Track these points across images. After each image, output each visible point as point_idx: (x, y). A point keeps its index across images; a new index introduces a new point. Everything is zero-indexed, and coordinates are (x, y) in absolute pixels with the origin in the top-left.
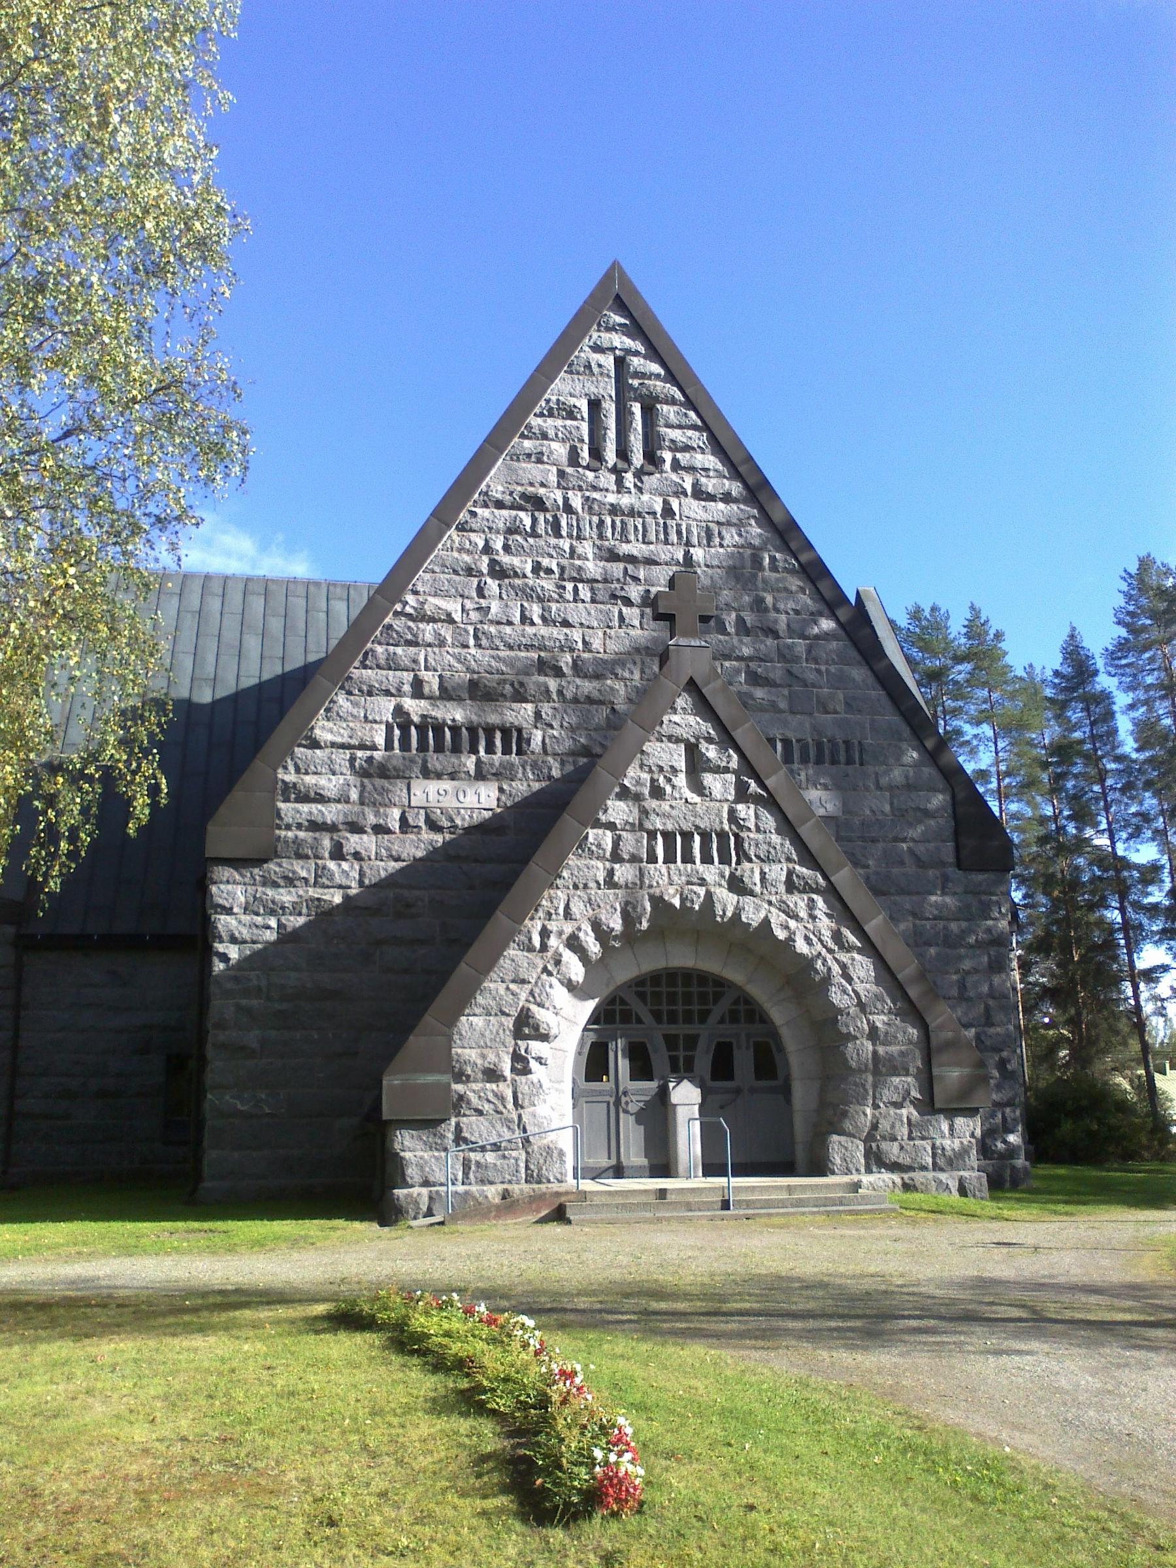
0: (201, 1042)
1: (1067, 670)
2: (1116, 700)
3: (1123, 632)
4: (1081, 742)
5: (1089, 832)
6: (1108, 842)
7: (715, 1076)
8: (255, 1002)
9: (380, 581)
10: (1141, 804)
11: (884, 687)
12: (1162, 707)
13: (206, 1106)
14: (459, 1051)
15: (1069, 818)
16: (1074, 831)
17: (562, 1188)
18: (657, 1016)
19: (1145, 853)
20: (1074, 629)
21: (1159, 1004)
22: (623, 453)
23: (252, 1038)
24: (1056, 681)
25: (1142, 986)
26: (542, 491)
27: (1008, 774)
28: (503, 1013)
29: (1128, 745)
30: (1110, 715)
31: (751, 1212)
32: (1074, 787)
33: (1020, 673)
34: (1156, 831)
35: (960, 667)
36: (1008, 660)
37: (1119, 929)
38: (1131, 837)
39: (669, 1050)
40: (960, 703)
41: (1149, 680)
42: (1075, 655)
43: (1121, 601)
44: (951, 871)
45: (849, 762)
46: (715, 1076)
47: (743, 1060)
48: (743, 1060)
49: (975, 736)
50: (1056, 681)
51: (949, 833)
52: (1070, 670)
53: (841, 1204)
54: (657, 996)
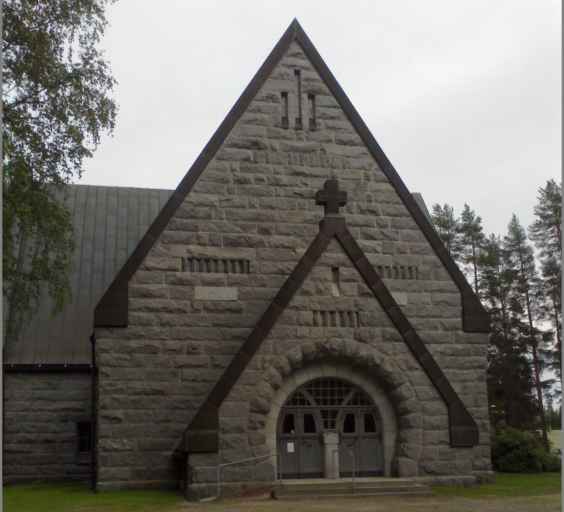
0: (94, 415)
2: (535, 252)
3: (538, 218)
5: (519, 316)
6: (528, 321)
8: (121, 396)
9: (175, 188)
12: (556, 255)
13: (98, 446)
15: (510, 309)
16: (512, 316)
17: (273, 483)
19: (546, 326)
20: (514, 216)
21: (549, 398)
22: (299, 120)
23: (119, 413)
24: (505, 242)
25: (542, 390)
26: (259, 139)
27: (481, 287)
29: (540, 275)
30: (531, 258)
31: (365, 494)
32: (513, 294)
34: (551, 315)
35: (458, 235)
37: (532, 363)
38: (539, 318)
40: (458, 253)
41: (550, 242)
42: (515, 228)
44: (461, 333)
45: (411, 278)
47: (359, 423)
48: (359, 423)
49: (466, 269)
50: (505, 242)
51: (459, 313)
52: (512, 236)
54: (317, 393)
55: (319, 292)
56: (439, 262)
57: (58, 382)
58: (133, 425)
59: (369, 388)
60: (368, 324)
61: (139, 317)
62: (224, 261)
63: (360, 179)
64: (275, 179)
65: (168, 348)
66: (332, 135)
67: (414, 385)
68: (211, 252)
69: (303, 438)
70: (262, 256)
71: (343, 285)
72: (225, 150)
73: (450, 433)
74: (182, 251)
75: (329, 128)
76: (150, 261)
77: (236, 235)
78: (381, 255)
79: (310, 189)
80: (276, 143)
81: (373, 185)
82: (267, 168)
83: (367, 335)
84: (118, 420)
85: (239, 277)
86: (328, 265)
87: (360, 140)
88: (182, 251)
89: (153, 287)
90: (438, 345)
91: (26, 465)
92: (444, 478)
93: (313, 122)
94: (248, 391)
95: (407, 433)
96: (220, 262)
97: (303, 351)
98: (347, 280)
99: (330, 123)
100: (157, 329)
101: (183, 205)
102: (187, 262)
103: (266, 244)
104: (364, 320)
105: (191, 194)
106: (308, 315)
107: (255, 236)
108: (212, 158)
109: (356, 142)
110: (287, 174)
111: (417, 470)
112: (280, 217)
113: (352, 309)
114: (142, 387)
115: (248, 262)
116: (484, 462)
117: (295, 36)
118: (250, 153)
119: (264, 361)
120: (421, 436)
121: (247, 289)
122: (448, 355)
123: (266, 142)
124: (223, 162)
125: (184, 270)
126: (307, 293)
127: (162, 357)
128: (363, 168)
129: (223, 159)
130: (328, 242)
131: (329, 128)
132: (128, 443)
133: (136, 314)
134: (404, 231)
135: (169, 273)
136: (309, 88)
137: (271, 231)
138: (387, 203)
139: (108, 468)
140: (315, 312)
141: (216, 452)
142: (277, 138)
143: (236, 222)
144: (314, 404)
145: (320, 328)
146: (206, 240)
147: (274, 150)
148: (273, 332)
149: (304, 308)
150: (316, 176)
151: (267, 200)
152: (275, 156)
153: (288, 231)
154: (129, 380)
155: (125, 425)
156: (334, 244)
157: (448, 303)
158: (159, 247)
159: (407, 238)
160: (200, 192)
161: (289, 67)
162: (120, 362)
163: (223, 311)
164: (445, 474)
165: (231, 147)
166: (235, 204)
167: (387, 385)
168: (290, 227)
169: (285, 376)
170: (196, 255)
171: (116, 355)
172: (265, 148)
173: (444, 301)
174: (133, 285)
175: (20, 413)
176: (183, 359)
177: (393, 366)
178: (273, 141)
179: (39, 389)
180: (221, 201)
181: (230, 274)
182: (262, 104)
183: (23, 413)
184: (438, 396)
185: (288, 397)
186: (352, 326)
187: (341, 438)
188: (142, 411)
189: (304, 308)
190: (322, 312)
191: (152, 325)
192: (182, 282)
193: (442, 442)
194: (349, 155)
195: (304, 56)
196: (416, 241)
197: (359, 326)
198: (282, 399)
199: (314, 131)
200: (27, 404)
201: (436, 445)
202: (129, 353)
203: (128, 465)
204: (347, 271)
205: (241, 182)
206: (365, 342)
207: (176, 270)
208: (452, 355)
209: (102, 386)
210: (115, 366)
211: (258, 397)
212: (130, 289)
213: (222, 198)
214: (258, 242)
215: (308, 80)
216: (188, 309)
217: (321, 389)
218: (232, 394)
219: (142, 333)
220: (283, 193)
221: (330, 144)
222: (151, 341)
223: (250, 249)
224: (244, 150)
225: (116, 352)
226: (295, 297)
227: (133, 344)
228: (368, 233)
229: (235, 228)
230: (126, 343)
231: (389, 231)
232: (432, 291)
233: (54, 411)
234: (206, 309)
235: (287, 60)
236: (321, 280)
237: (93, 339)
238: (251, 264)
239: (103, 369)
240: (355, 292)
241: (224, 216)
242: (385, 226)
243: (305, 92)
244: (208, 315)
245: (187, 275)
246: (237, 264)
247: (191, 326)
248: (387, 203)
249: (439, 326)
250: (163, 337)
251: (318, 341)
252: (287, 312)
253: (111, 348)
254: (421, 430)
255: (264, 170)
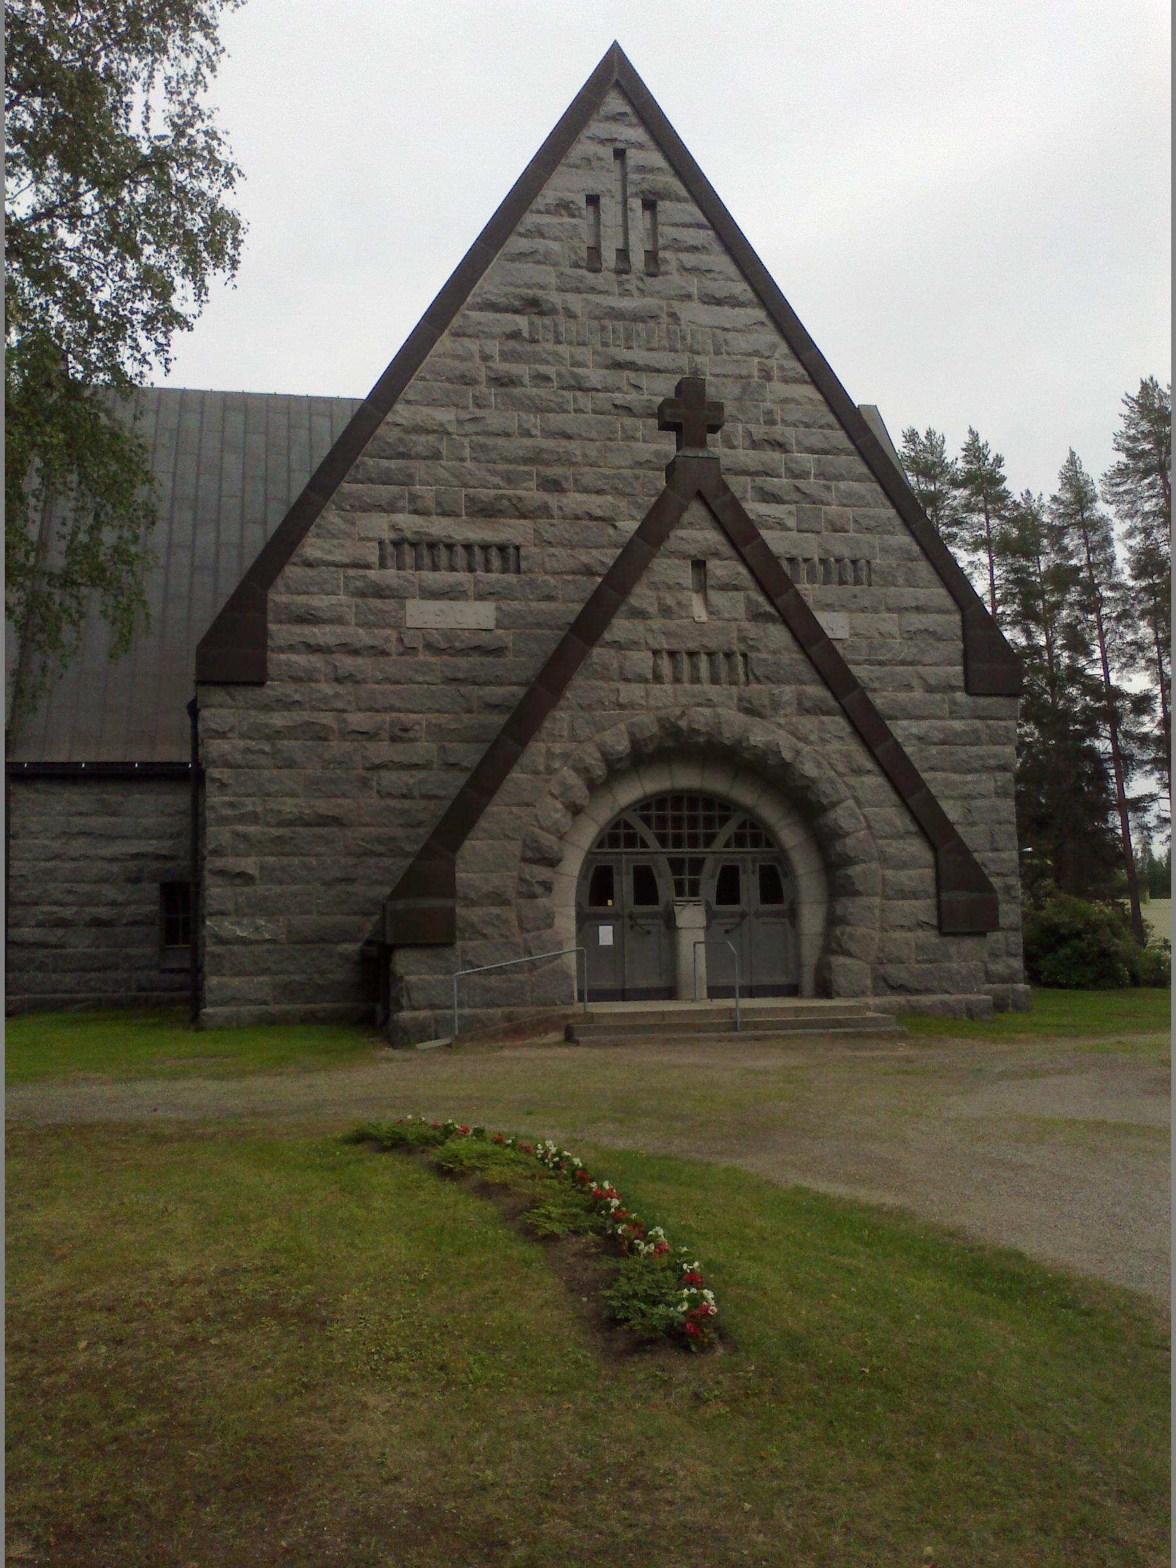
0: (196, 868)
1: (1067, 496)
2: (1115, 527)
3: (1122, 458)
4: (1078, 569)
6: (1101, 672)
7: (721, 900)
8: (252, 829)
9: (363, 394)
10: (1136, 633)
11: (895, 505)
13: (205, 933)
14: (463, 875)
15: (1063, 647)
16: (1067, 661)
17: (569, 1010)
18: (662, 840)
19: (1137, 682)
20: (1073, 454)
21: (1145, 832)
22: (623, 254)
23: (248, 864)
24: (1054, 507)
25: (1130, 815)
26: (540, 293)
28: (508, 837)
29: (1125, 576)
30: (1107, 541)
31: (760, 1033)
33: (1018, 498)
34: (1150, 660)
35: (956, 493)
36: (1007, 485)
37: (1110, 759)
39: (674, 873)
41: (1148, 507)
43: (1121, 425)
44: (960, 696)
45: (857, 582)
46: (721, 900)
47: (750, 885)
48: (750, 885)
49: (971, 563)
50: (1054, 507)
51: (958, 656)
52: (1068, 495)
53: (849, 1026)
54: (662, 820)
55: (666, 612)
56: (915, 549)
57: (121, 799)
58: (277, 889)
59: (771, 813)
60: (767, 678)
61: (289, 664)
62: (468, 547)
63: (750, 377)
64: (574, 376)
65: (350, 728)
66: (693, 285)
67: (864, 806)
68: (439, 527)
69: (631, 917)
70: (546, 536)
71: (719, 599)
72: (470, 315)
73: (939, 907)
74: (379, 525)
75: (686, 269)
76: (312, 547)
77: (493, 492)
78: (794, 534)
79: (646, 397)
80: (575, 302)
81: (777, 388)
82: (556, 354)
83: (766, 702)
84: (245, 878)
85: (498, 581)
86: (684, 556)
87: (750, 295)
88: (379, 525)
89: (320, 602)
90: (914, 723)
91: (54, 972)
92: (926, 1000)
93: (652, 256)
94: (519, 818)
95: (849, 906)
96: (460, 550)
97: (631, 734)
98: (724, 587)
99: (689, 259)
100: (327, 689)
101: (381, 430)
102: (390, 549)
103: (556, 512)
104: (759, 671)
105: (399, 407)
106: (641, 660)
107: (532, 494)
108: (442, 332)
109: (741, 299)
110: (598, 366)
111: (869, 982)
112: (585, 455)
113: (735, 648)
114: (295, 810)
115: (517, 548)
116: (1009, 966)
117: (615, 77)
118: (522, 322)
119: (550, 755)
120: (877, 912)
121: (516, 605)
122: (935, 744)
123: (555, 298)
124: (466, 340)
125: (383, 565)
126: (640, 614)
127: (338, 747)
128: (756, 353)
129: (465, 335)
130: (684, 508)
131: (686, 269)
132: (267, 927)
133: (283, 657)
134: (843, 485)
135: (352, 572)
136: (645, 186)
137: (565, 485)
138: (807, 425)
139: (225, 980)
140: (656, 653)
141: (450, 944)
142: (578, 291)
143: (491, 466)
144: (654, 845)
145: (668, 687)
146: (431, 504)
147: (570, 315)
148: (568, 694)
149: (634, 645)
150: (659, 371)
151: (556, 420)
152: (574, 328)
153: (600, 484)
154: (269, 795)
155: (261, 889)
156: (696, 510)
157: (933, 634)
158: (332, 517)
159: (848, 500)
160: (417, 403)
161: (603, 142)
162: (250, 757)
163: (465, 652)
164: (929, 991)
165: (481, 309)
166: (490, 428)
167: (806, 805)
168: (605, 477)
169: (594, 787)
170: (408, 535)
171: (242, 743)
172: (553, 311)
173: (926, 630)
174: (278, 597)
175: (43, 864)
176: (381, 751)
177: (819, 766)
178: (569, 296)
179: (80, 814)
180: (460, 422)
181: (480, 573)
182: (546, 219)
183: (49, 865)
184: (913, 828)
185: (602, 830)
186: (733, 683)
187: (711, 915)
188: (296, 860)
189: (634, 645)
190: (672, 654)
191: (317, 681)
192: (379, 592)
193: (921, 925)
194: (728, 326)
195: (634, 120)
196: (868, 505)
197: (747, 682)
198: (587, 833)
199: (654, 275)
200: (56, 845)
201: (910, 929)
202: (268, 738)
203: (266, 971)
204: (723, 569)
205: (502, 382)
206: (761, 715)
207: (368, 566)
208: (943, 743)
209: (212, 808)
210: (239, 767)
211: (538, 831)
212: (270, 605)
213: (464, 416)
214: (539, 508)
215: (641, 169)
216: (392, 647)
217: (701, 813)
218: (484, 823)
219: (297, 697)
220: (590, 406)
221: (687, 304)
222: (315, 714)
223: (522, 521)
224: (509, 316)
225: (243, 736)
226: (615, 621)
227: (278, 720)
228: (768, 488)
229: (489, 478)
230: (262, 718)
231: (811, 485)
232: (901, 610)
233: (112, 860)
234: (430, 647)
235: (598, 128)
236: (669, 588)
237: (193, 710)
238: (523, 552)
239: (214, 772)
240: (741, 612)
241: (467, 453)
242: (804, 475)
243: (636, 195)
244: (434, 659)
245: (390, 576)
246: (494, 552)
247: (397, 682)
248: (807, 425)
249: (915, 682)
250: (339, 705)
251: (662, 713)
252: (598, 654)
253: (232, 729)
254: (877, 900)
255: (550, 358)
